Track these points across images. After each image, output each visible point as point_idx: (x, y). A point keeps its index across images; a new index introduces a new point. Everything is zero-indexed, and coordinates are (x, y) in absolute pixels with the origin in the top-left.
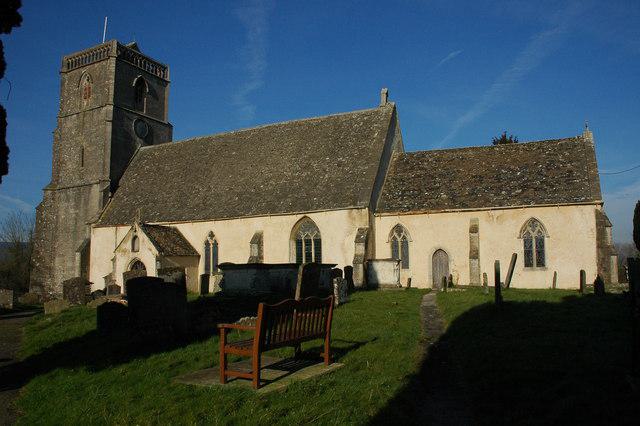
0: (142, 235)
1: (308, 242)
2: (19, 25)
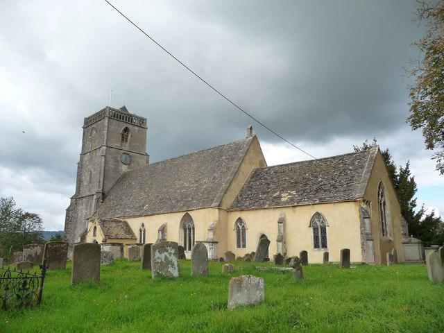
0: (99, 228)
1: (190, 229)
2: (124, 108)
